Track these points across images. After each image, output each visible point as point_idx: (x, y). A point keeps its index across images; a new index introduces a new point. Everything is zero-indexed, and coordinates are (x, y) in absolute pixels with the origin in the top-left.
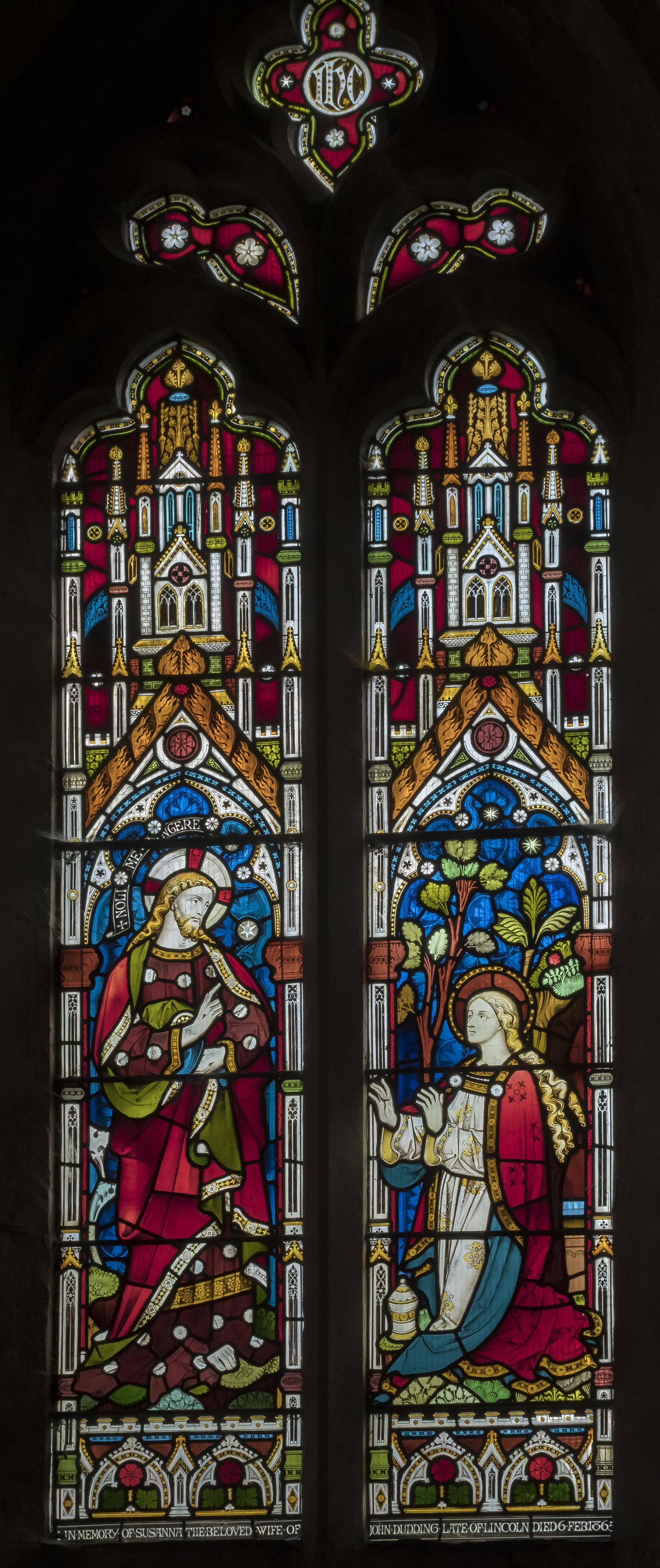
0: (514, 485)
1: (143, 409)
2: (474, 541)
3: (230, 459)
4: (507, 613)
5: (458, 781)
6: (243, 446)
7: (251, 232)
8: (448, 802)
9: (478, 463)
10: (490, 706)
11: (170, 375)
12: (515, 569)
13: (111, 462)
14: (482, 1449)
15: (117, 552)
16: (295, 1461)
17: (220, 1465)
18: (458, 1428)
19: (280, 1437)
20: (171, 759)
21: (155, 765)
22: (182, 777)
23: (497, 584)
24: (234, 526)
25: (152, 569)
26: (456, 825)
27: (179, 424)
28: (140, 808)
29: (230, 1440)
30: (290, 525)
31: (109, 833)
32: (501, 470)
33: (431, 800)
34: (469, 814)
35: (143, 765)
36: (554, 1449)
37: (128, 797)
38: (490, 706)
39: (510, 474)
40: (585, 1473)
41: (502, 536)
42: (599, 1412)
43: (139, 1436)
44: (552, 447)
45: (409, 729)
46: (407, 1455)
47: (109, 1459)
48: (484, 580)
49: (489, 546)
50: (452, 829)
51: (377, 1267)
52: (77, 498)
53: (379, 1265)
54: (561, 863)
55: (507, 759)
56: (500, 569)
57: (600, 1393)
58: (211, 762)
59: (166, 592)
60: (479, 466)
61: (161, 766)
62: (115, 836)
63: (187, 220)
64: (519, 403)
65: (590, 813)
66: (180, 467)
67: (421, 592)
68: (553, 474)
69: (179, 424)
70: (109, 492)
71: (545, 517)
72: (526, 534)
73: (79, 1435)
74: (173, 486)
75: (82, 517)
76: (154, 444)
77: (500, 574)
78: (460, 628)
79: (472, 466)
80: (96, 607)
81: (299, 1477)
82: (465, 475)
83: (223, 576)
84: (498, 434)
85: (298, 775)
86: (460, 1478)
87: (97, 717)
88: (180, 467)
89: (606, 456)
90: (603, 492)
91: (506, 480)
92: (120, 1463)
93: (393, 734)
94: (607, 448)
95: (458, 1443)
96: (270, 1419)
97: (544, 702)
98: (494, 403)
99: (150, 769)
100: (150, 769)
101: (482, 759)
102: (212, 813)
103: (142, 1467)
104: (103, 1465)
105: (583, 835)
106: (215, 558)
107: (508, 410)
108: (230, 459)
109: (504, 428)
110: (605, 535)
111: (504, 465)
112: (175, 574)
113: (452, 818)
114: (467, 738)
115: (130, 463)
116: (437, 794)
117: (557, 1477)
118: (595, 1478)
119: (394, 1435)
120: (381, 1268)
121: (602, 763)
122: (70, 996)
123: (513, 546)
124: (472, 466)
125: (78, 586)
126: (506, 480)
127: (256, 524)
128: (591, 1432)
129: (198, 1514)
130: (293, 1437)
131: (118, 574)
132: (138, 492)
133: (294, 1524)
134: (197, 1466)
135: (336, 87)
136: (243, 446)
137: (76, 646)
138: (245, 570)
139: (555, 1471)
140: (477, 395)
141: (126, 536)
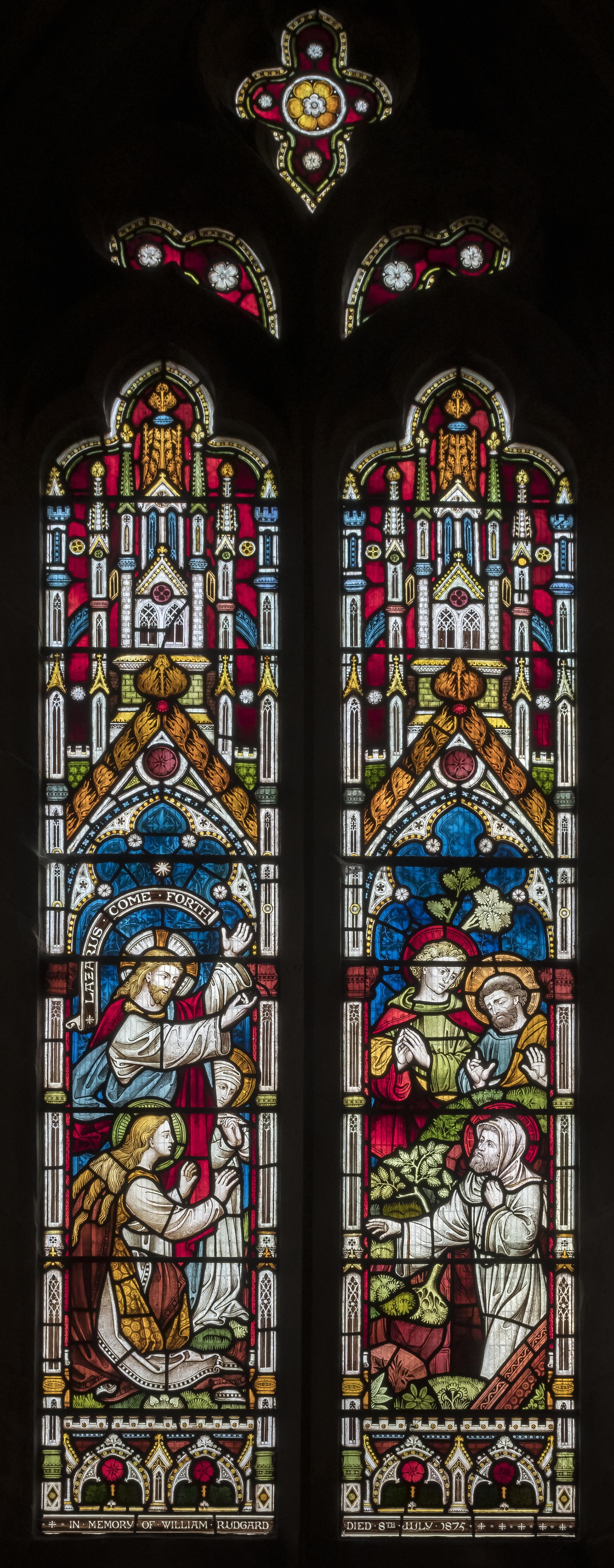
0: (188, 516)
1: (126, 428)
2: (442, 575)
3: (508, 487)
4: (180, 638)
6: (522, 477)
7: (230, 258)
8: (121, 822)
9: (153, 492)
11: (450, 404)
12: (485, 601)
13: (93, 479)
14: (149, 1451)
15: (98, 567)
16: (566, 1463)
17: (103, 1462)
19: (551, 1438)
20: (449, 779)
24: (511, 555)
26: (427, 851)
27: (459, 452)
28: (500, 827)
29: (205, 1440)
30: (266, 550)
31: (390, 846)
32: (175, 500)
33: (400, 826)
34: (440, 840)
37: (408, 815)
39: (184, 505)
42: (560, 1421)
44: (227, 479)
45: (549, 757)
46: (80, 1455)
48: (158, 607)
49: (161, 574)
50: (423, 854)
51: (349, 1277)
52: (62, 514)
54: (394, 891)
56: (174, 596)
59: (446, 617)
60: (155, 495)
62: (396, 851)
63: (161, 243)
64: (489, 442)
66: (458, 493)
67: (95, 615)
68: (522, 513)
69: (459, 452)
73: (363, 1432)
74: (173, 504)
75: (66, 532)
76: (137, 463)
77: (172, 603)
78: (133, 651)
79: (148, 494)
80: (81, 620)
82: (140, 505)
83: (501, 603)
86: (187, 1478)
87: (78, 728)
88: (458, 493)
90: (567, 535)
91: (476, 516)
93: (70, 754)
94: (571, 489)
95: (127, 1445)
97: (513, 735)
99: (428, 788)
100: (428, 788)
102: (485, 834)
103: (424, 1464)
104: (88, 1458)
105: (551, 866)
107: (182, 442)
108: (508, 487)
109: (178, 459)
111: (177, 494)
113: (423, 843)
115: (112, 481)
116: (112, 814)
117: (218, 1481)
122: (54, 1003)
124: (148, 494)
125: (359, 604)
126: (476, 516)
128: (551, 1438)
129: (82, 1509)
131: (99, 590)
132: (417, 514)
134: (380, 1465)
136: (522, 477)
137: (357, 664)
139: (425, 1476)
140: (447, 431)
141: (107, 551)
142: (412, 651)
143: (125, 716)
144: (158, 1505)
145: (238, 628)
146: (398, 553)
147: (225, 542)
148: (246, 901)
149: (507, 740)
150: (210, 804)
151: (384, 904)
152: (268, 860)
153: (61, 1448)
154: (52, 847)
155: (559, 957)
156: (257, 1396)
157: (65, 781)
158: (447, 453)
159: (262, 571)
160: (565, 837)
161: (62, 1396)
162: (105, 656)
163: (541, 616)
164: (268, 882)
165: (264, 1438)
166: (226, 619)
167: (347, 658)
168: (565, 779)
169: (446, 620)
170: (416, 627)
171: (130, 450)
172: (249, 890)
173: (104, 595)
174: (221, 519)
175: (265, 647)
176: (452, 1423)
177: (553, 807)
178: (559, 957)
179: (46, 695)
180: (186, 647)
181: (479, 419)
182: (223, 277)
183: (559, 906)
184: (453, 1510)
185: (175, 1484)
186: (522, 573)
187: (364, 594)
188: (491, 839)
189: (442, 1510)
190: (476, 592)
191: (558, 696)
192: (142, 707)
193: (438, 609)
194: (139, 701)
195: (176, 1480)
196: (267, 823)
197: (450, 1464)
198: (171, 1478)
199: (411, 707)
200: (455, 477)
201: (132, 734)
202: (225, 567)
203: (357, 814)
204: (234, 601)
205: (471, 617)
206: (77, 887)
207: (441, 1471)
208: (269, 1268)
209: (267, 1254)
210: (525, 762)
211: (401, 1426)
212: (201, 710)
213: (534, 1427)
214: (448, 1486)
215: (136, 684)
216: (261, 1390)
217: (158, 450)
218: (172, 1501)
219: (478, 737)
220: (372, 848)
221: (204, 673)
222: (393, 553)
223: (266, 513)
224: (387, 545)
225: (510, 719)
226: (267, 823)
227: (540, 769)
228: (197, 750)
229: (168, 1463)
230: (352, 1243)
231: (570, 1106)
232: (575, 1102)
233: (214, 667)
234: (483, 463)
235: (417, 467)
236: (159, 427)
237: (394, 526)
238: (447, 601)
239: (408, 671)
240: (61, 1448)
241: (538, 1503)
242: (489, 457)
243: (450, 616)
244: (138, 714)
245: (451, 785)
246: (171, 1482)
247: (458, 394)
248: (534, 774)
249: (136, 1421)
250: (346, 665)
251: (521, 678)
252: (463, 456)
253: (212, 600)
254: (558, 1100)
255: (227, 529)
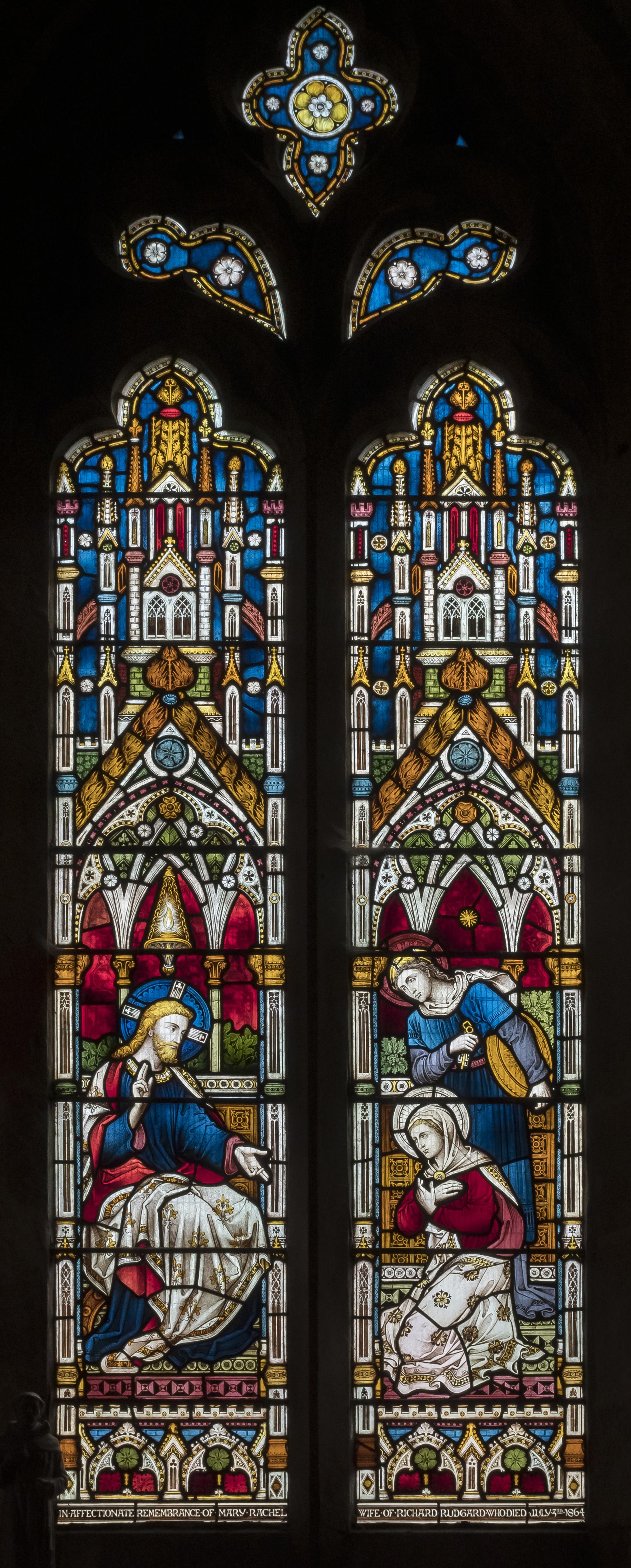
5: (138, 794)
10: (171, 726)
12: (490, 591)
15: (401, 562)
18: (439, 1420)
19: (264, 1425)
21: (144, 771)
22: (468, 788)
23: (178, 603)
25: (142, 578)
28: (506, 817)
35: (134, 769)
36: (436, 1441)
38: (171, 726)
40: (555, 1463)
41: (184, 558)
43: (432, 1422)
47: (498, 1442)
53: (64, 1262)
55: (479, 779)
57: (569, 1390)
58: (490, 775)
59: (451, 606)
61: (150, 774)
65: (560, 836)
70: (394, 504)
71: (226, 541)
72: (206, 556)
77: (181, 594)
78: (141, 643)
81: (581, 1465)
84: (179, 456)
85: (280, 788)
89: (282, 484)
90: (571, 523)
92: (117, 1446)
93: (80, 746)
94: (576, 478)
96: (257, 1409)
98: (176, 427)
101: (162, 774)
106: (205, 570)
109: (479, 455)
110: (278, 562)
112: (459, 587)
114: (148, 755)
118: (565, 1470)
119: (81, 1426)
120: (66, 1265)
121: (275, 786)
122: (62, 994)
123: (195, 567)
127: (538, 543)
130: (575, 1426)
133: (209, 1508)
135: (322, 108)
138: (233, 583)
139: (231, 1463)
142: (418, 643)
143: (430, 708)
144: (471, 1494)
145: (539, 621)
146: (404, 545)
147: (234, 534)
148: (254, 891)
149: (218, 727)
150: (218, 797)
151: (92, 891)
152: (275, 849)
153: (76, 1438)
154: (61, 841)
155: (270, 942)
156: (565, 1385)
157: (74, 773)
158: (452, 443)
159: (268, 562)
160: (275, 822)
161: (373, 1385)
162: (533, 651)
163: (549, 605)
164: (275, 874)
165: (575, 1426)
166: (527, 614)
167: (355, 649)
168: (275, 764)
169: (452, 608)
170: (128, 616)
171: (432, 447)
172: (256, 880)
173: (407, 591)
174: (395, 514)
175: (271, 639)
176: (184, 1410)
177: (559, 797)
178: (270, 942)
179: (351, 691)
180: (194, 639)
181: (189, 408)
182: (228, 272)
183: (270, 891)
184: (466, 1496)
185: (487, 1474)
186: (402, 562)
187: (371, 586)
188: (498, 828)
189: (455, 1497)
190: (480, 580)
191: (396, 683)
192: (446, 702)
193: (443, 599)
194: (148, 695)
195: (488, 1470)
196: (571, 814)
197: (463, 1450)
198: (483, 1467)
199: (123, 694)
200: (460, 467)
201: (437, 729)
202: (526, 562)
203: (69, 801)
204: (242, 591)
205: (476, 606)
206: (83, 877)
207: (455, 1459)
208: (68, 1258)
209: (364, 1244)
210: (234, 747)
211: (183, 1414)
212: (504, 704)
213: (546, 1413)
214: (460, 1475)
215: (145, 678)
216: (569, 1380)
217: (165, 442)
218: (485, 1489)
219: (482, 728)
220: (82, 836)
221: (506, 667)
222: (399, 544)
223: (565, 510)
224: (394, 537)
225: (220, 707)
226: (571, 814)
227: (380, 757)
228: (503, 744)
229: (181, 1451)
230: (363, 1231)
231: (281, 1093)
232: (286, 1088)
233: (515, 661)
234: (488, 455)
235: (130, 455)
236: (460, 424)
237: (527, 517)
238: (453, 591)
239: (120, 660)
240: (76, 1438)
241: (457, 1488)
242: (494, 448)
243: (456, 604)
244: (145, 707)
245: (162, 774)
246: (483, 1472)
247: (171, 383)
248: (541, 763)
249: (465, 1410)
250: (354, 655)
251: (232, 664)
252: (468, 446)
253: (514, 593)
254: (269, 1086)
255: (402, 524)
